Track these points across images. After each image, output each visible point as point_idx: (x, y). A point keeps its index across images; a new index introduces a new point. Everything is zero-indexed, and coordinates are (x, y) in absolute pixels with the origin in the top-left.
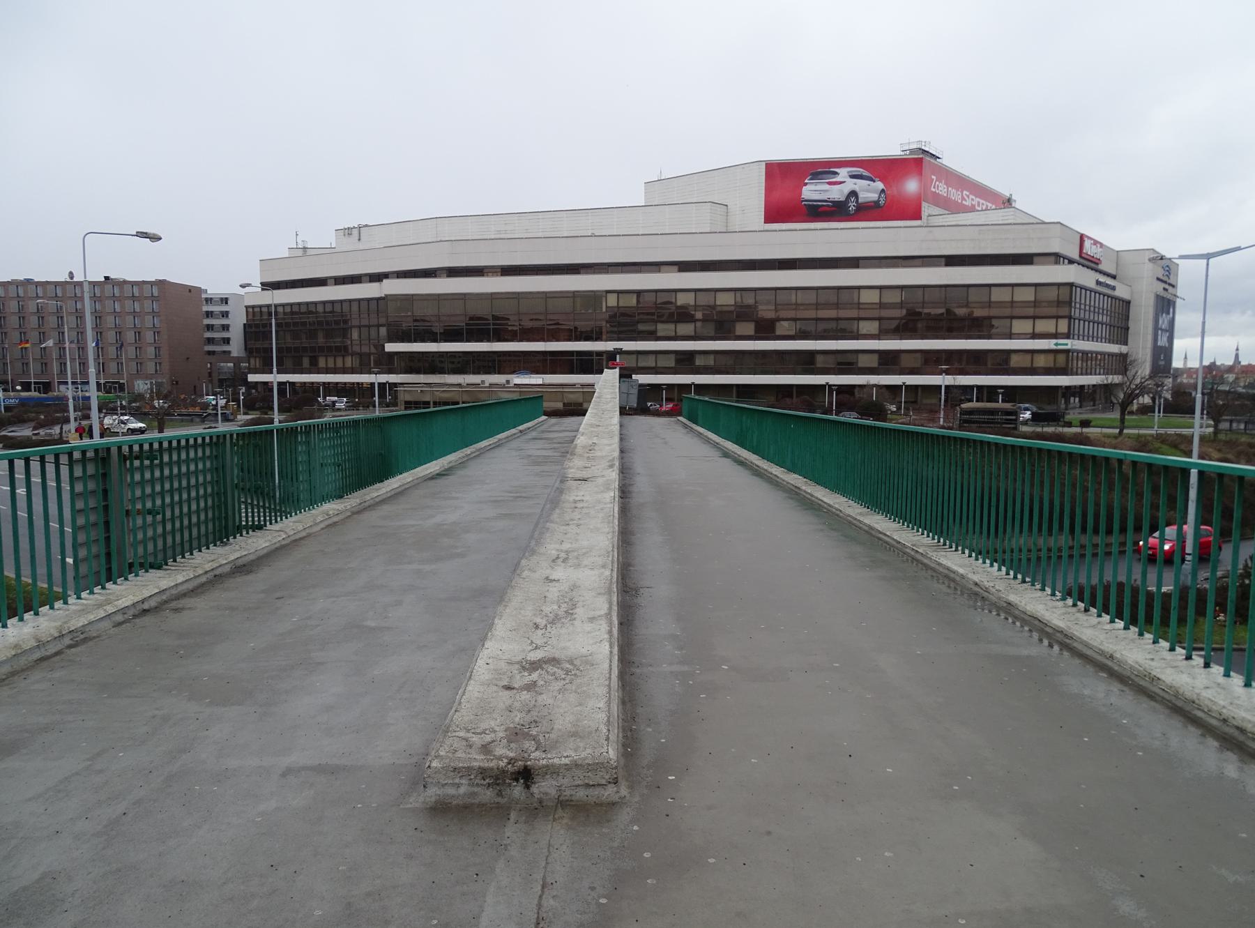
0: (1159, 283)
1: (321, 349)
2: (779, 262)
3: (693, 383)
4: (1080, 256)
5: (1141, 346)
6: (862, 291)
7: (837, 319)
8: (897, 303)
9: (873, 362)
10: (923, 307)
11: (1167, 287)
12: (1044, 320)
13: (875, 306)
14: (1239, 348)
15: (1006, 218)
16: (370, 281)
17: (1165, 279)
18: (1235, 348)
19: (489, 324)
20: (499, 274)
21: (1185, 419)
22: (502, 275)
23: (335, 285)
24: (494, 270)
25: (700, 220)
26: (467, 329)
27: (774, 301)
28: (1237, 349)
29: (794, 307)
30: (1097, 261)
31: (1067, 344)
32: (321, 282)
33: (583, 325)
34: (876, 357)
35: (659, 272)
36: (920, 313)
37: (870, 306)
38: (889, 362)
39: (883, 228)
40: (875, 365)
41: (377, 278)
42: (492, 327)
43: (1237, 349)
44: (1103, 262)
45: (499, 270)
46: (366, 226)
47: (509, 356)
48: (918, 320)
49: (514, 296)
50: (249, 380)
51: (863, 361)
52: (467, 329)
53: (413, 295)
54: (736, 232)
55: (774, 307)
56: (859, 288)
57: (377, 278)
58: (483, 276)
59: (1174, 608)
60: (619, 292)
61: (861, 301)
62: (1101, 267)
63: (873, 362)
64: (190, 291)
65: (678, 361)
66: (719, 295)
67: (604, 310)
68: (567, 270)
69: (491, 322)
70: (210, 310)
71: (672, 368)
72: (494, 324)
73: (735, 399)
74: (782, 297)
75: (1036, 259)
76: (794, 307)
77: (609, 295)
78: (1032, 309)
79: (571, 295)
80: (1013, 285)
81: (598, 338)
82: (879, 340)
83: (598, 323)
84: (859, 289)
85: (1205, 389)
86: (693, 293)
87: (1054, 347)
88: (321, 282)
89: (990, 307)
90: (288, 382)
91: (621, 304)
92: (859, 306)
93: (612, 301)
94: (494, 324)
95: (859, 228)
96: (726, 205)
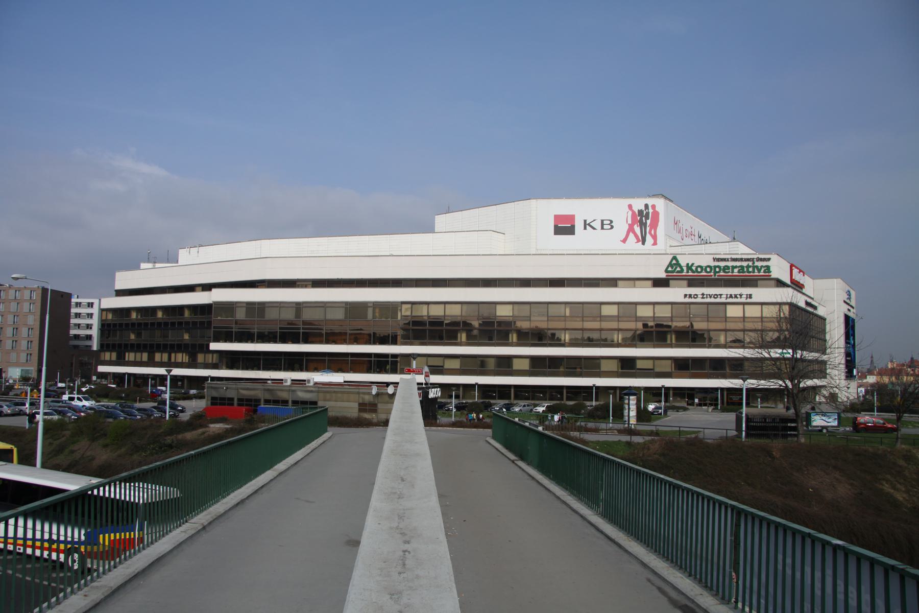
0: (845, 305)
1: (158, 346)
3: (477, 384)
4: (791, 282)
6: (639, 307)
7: (601, 330)
8: (651, 317)
9: (525, 365)
10: (672, 321)
11: (850, 308)
12: (589, 328)
13: (756, 320)
14: (873, 356)
17: (848, 301)
18: (871, 356)
19: (299, 329)
20: (311, 286)
21: (591, 402)
26: (280, 332)
27: (546, 313)
28: (872, 357)
29: (563, 318)
30: (801, 286)
32: (190, 288)
33: (381, 331)
34: (527, 361)
35: (634, 286)
36: (669, 327)
37: (753, 320)
38: (627, 366)
40: (668, 370)
41: (207, 287)
42: (301, 331)
43: (872, 357)
44: (805, 287)
45: (311, 283)
48: (668, 331)
51: (605, 366)
52: (280, 332)
55: (546, 319)
56: (636, 304)
57: (207, 287)
59: (226, 503)
60: (413, 303)
61: (602, 314)
62: (804, 291)
63: (667, 367)
64: (62, 296)
65: (599, 366)
66: (603, 307)
67: (399, 318)
68: (343, 284)
69: (301, 326)
70: (79, 312)
71: (528, 370)
72: (303, 329)
73: (876, 413)
74: (553, 310)
75: (620, 283)
77: (404, 306)
78: (706, 323)
80: (445, 303)
81: (394, 342)
82: (636, 348)
84: (583, 304)
86: (778, 306)
88: (190, 288)
89: (744, 321)
91: (413, 314)
92: (602, 318)
93: (406, 311)
94: (303, 329)
95: (651, 254)
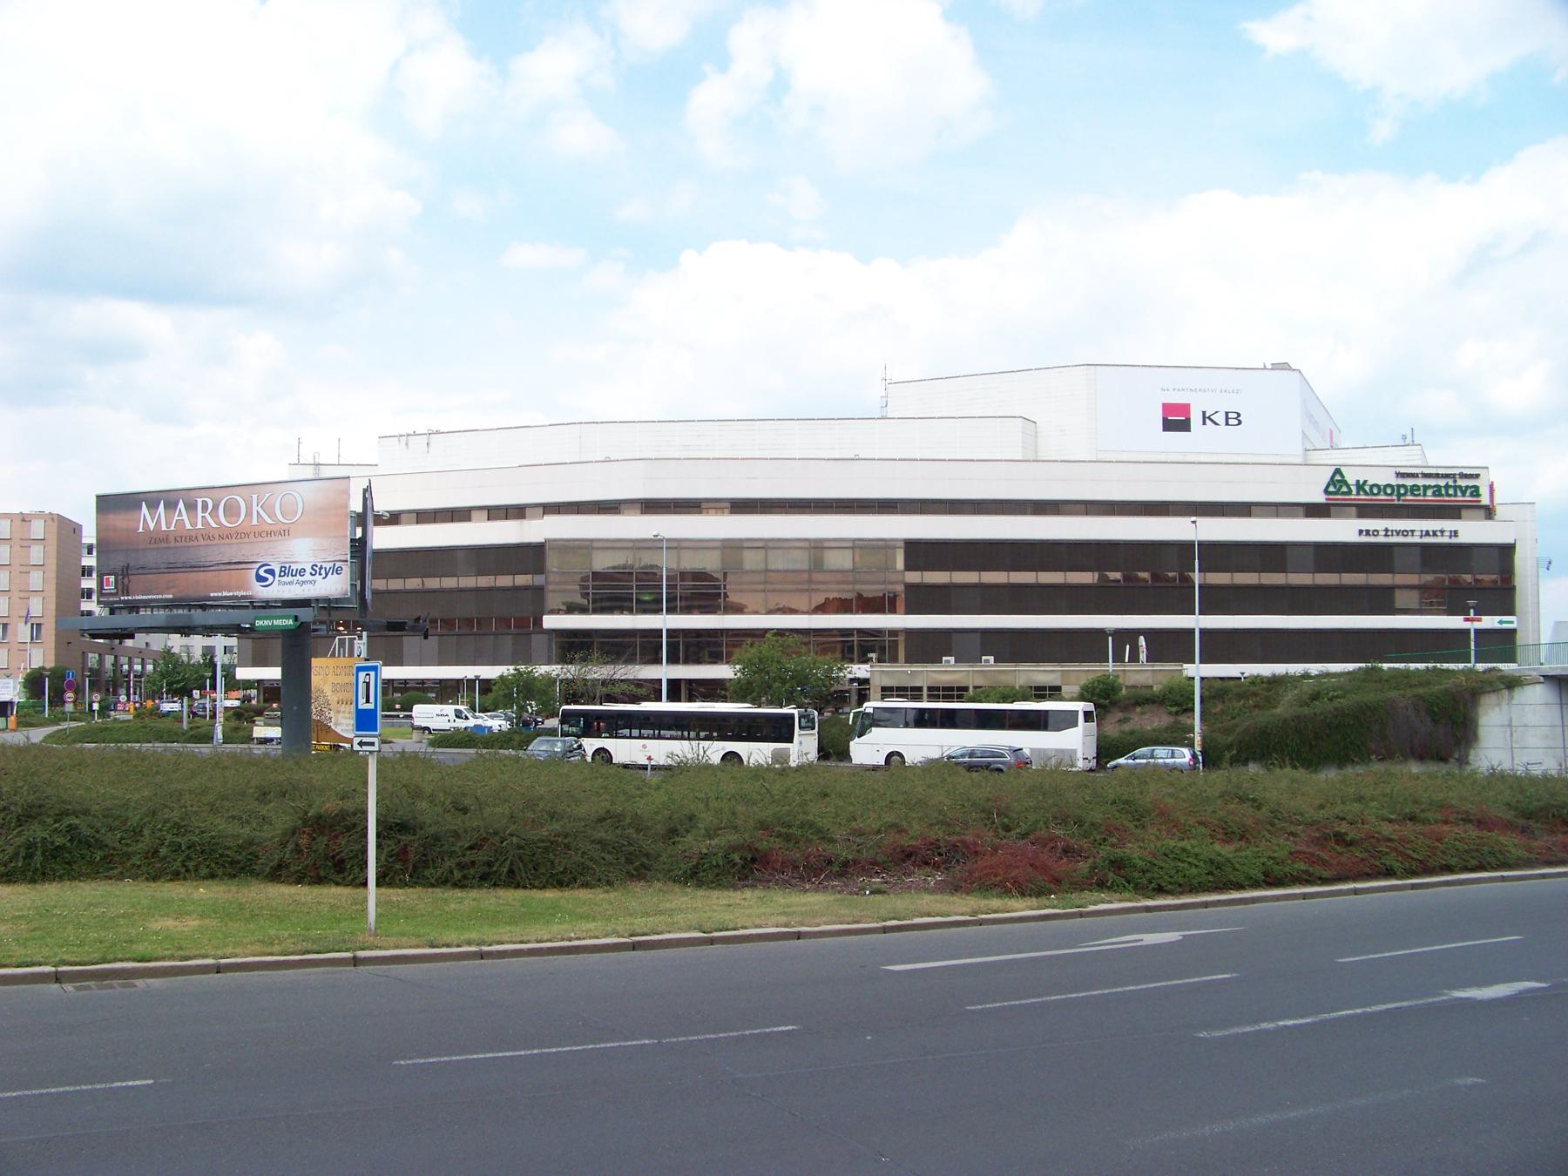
2: (1145, 505)
5: (1530, 629)
15: (1412, 458)
16: (732, 512)
22: (731, 513)
23: (417, 523)
24: (718, 505)
25: (1008, 442)
31: (1512, 622)
39: (1116, 462)
46: (438, 432)
47: (710, 636)
49: (760, 544)
50: (238, 677)
53: (592, 541)
54: (795, 459)
57: (516, 512)
58: (700, 513)
76: (761, 578)
79: (719, 544)
83: (891, 587)
85: (929, 714)
87: (1498, 626)
90: (477, 678)
96: (1035, 423)
